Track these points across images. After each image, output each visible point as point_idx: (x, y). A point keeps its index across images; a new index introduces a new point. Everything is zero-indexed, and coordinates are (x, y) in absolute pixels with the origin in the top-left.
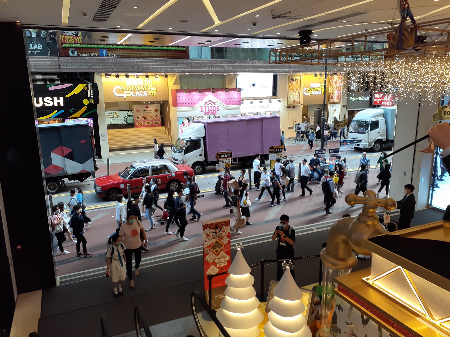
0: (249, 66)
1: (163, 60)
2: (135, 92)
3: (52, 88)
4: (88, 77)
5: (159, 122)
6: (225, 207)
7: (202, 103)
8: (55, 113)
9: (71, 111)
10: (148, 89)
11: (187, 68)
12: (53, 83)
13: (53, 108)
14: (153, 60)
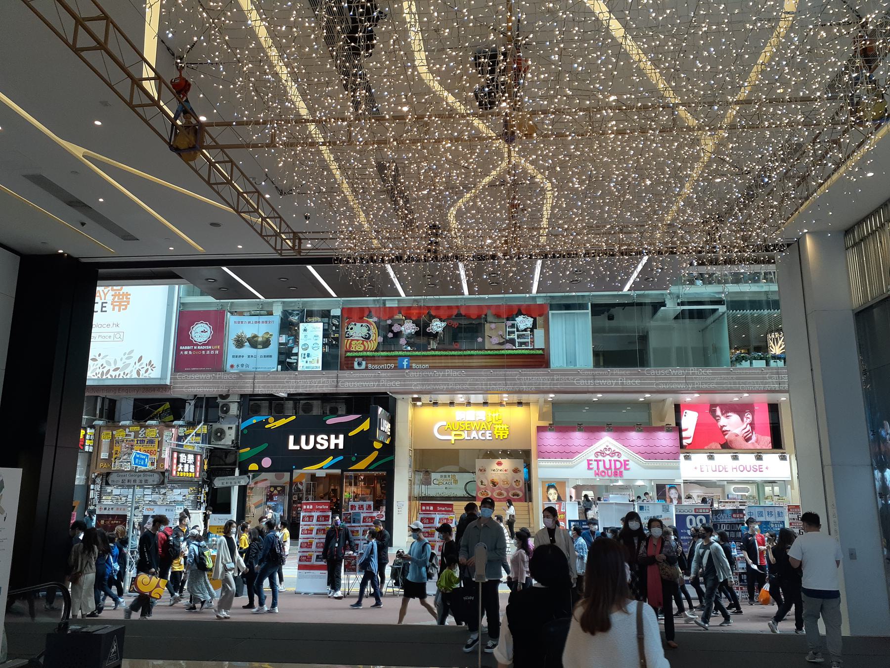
0: (677, 379)
1: (501, 372)
2: (469, 433)
3: (331, 421)
4: (387, 401)
5: (521, 494)
7: (590, 453)
8: (329, 461)
9: (354, 459)
10: (492, 429)
11: (543, 384)
12: (334, 412)
13: (327, 452)
14: (483, 372)
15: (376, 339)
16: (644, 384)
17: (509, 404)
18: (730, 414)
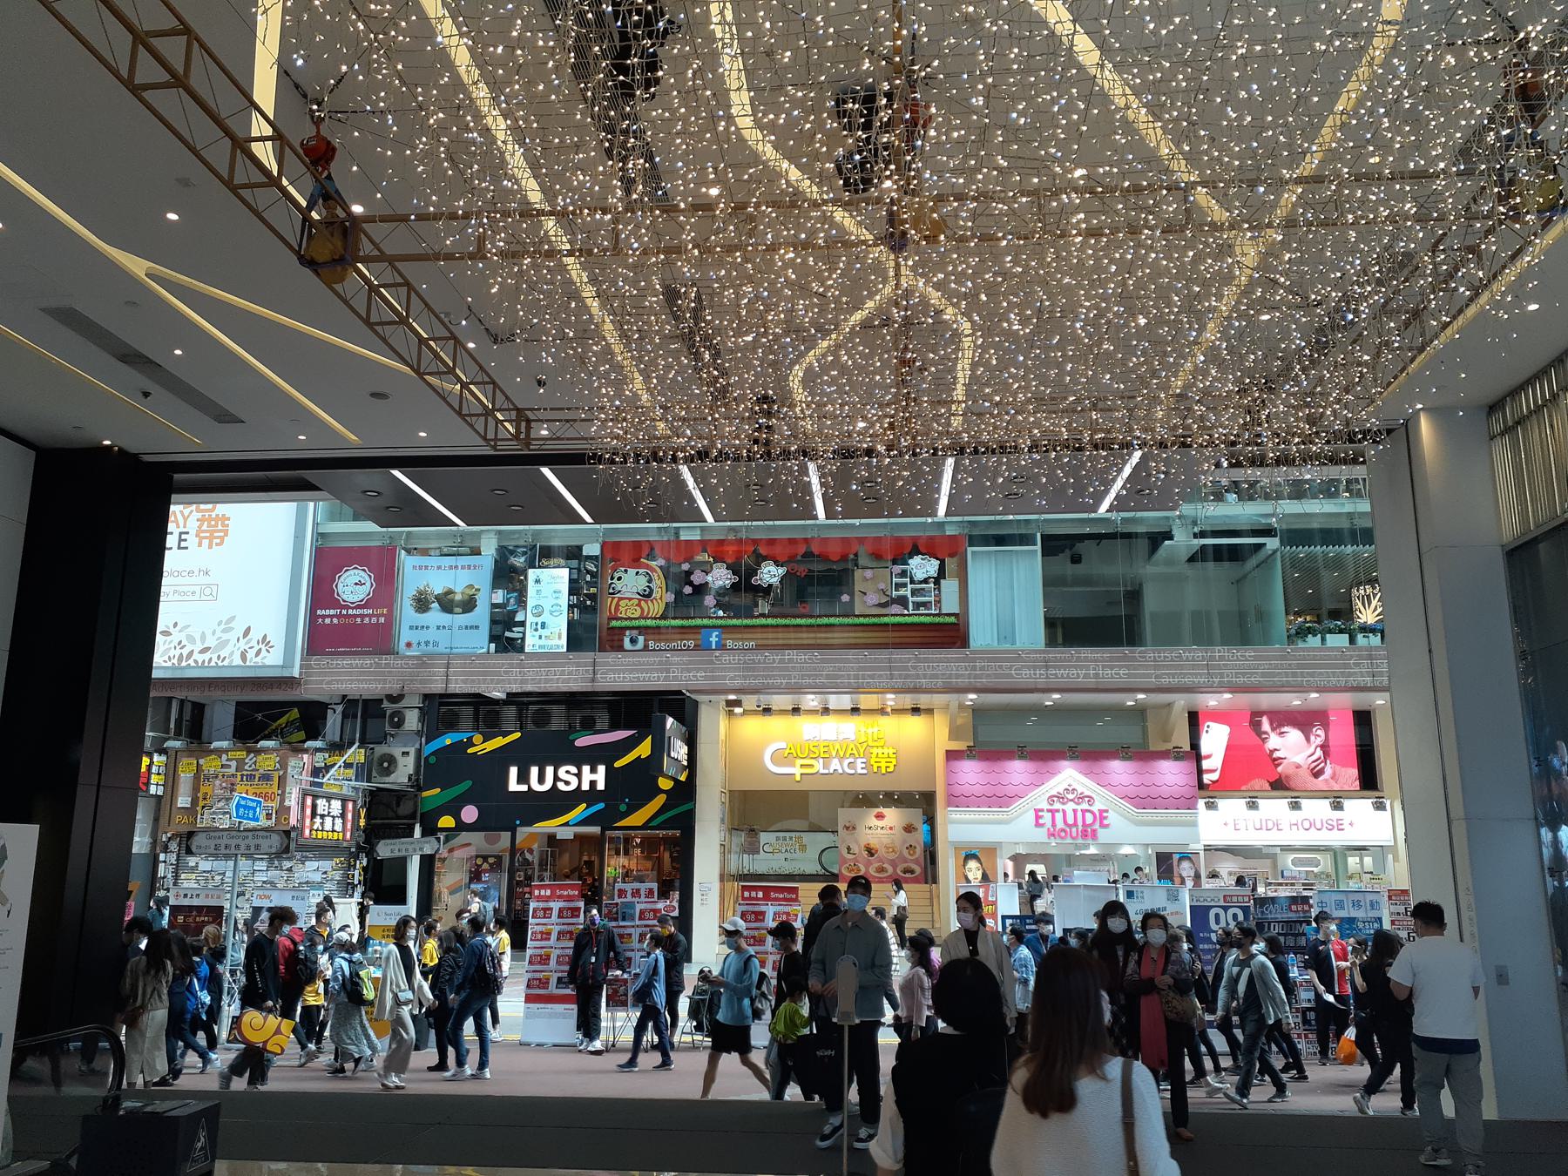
0: (1193, 667)
1: (883, 654)
2: (827, 761)
3: (583, 741)
4: (682, 706)
5: (918, 870)
6: (430, 1069)
7: (1039, 798)
8: (580, 811)
9: (623, 808)
10: (867, 754)
11: (958, 676)
12: (589, 726)
13: (577, 796)
14: (851, 654)
15: (663, 597)
16: (1135, 676)
17: (896, 711)
18: (1285, 729)
